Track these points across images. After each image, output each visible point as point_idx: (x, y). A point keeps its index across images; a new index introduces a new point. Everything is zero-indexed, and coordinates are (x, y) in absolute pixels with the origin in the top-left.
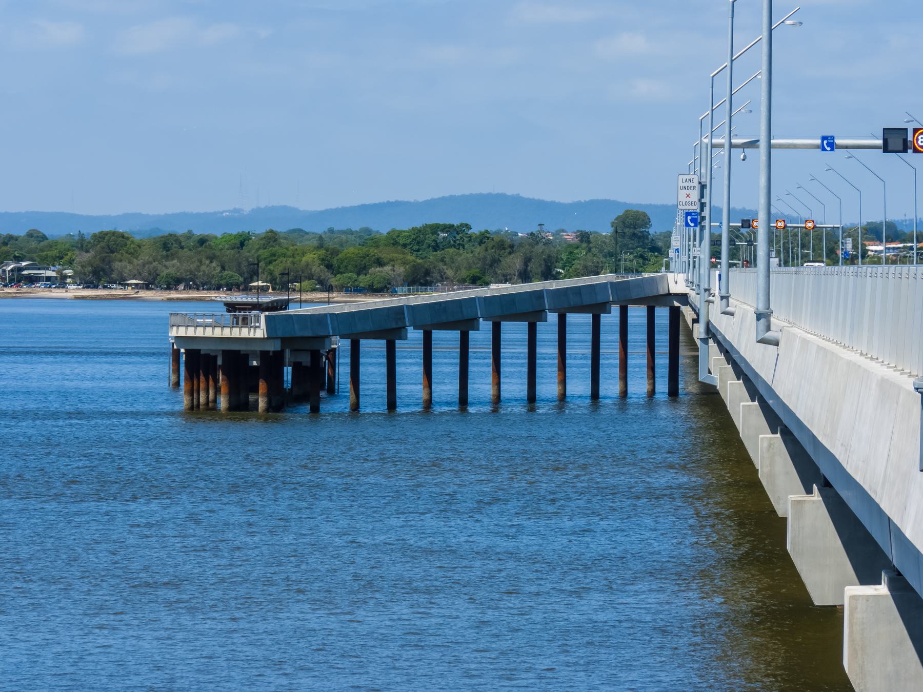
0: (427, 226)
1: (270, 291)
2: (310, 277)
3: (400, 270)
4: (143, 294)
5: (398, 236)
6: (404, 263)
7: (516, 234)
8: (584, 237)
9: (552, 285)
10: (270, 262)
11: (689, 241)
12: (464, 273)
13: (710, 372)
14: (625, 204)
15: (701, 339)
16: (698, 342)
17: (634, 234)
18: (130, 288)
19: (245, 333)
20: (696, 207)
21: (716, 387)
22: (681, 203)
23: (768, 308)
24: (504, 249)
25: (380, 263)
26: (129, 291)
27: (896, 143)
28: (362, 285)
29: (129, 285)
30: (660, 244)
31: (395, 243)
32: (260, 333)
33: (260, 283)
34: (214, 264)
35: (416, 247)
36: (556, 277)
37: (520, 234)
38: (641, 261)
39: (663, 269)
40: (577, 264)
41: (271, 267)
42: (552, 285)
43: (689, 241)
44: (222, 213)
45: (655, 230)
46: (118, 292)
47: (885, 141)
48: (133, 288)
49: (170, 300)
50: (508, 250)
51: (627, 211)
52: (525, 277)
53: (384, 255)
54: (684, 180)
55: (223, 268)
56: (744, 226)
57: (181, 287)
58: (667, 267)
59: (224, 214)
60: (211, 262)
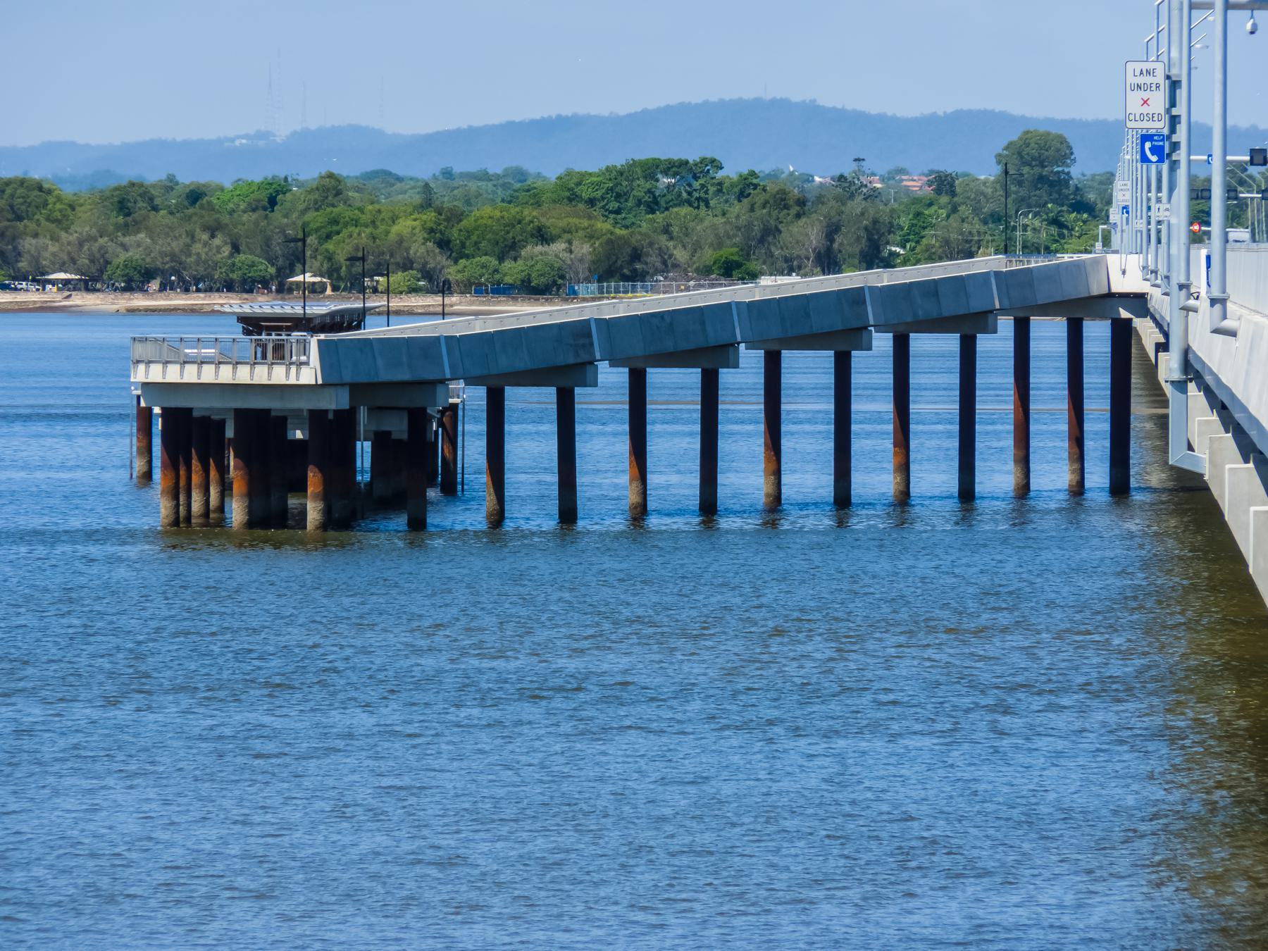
0: (634, 164)
1: (329, 291)
2: (406, 265)
3: (584, 249)
4: (80, 300)
7: (809, 178)
8: (944, 184)
9: (882, 278)
10: (329, 237)
11: (1149, 191)
12: (708, 255)
13: (1190, 448)
14: (1023, 119)
15: (1172, 382)
16: (1168, 389)
19: (279, 375)
20: (1160, 124)
21: (1202, 475)
22: (1132, 117)
24: (787, 207)
25: (543, 236)
27: (1257, 159)
29: (53, 283)
31: (573, 198)
33: (309, 278)
34: (217, 241)
35: (614, 205)
36: (888, 263)
37: (817, 179)
39: (1099, 245)
40: (931, 238)
41: (330, 246)
42: (882, 278)
43: (1149, 191)
44: (233, 140)
45: (1080, 170)
50: (793, 211)
51: (1027, 132)
52: (828, 262)
53: (554, 219)
54: (1138, 73)
55: (236, 249)
56: (1255, 162)
59: (237, 143)
60: (213, 236)
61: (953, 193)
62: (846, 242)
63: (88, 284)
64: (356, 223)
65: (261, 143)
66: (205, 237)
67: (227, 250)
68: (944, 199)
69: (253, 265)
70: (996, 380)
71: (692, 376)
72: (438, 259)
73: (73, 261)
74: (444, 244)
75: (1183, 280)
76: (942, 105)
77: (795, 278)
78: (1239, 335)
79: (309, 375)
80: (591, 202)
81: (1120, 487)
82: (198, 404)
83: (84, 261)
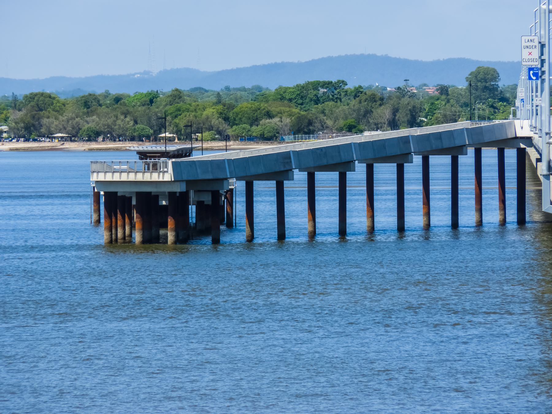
0: (309, 83)
1: (176, 140)
2: (210, 129)
3: (287, 121)
4: (68, 145)
5: (285, 92)
6: (290, 115)
7: (385, 89)
8: (444, 90)
9: (417, 131)
10: (176, 117)
12: (341, 123)
14: (478, 62)
15: (543, 175)
16: (541, 178)
18: (57, 141)
19: (155, 177)
24: (375, 101)
25: (269, 115)
26: (56, 143)
28: (254, 134)
29: (55, 138)
31: (282, 98)
32: (168, 177)
33: (168, 135)
34: (128, 119)
36: (420, 125)
37: (388, 89)
38: (492, 110)
39: (511, 116)
40: (438, 114)
41: (177, 120)
42: (417, 131)
43: (532, 92)
44: (134, 75)
45: (503, 83)
46: (46, 144)
48: (59, 141)
49: (91, 150)
50: (378, 103)
51: (479, 68)
52: (394, 125)
55: (136, 122)
57: (100, 139)
58: (515, 114)
59: (136, 76)
60: (126, 117)
62: (402, 116)
63: (71, 138)
67: (132, 123)
69: (143, 129)
72: (224, 126)
73: (65, 128)
74: (226, 119)
75: (547, 131)
77: (379, 132)
79: (168, 177)
80: (290, 100)
81: (521, 221)
82: (121, 191)
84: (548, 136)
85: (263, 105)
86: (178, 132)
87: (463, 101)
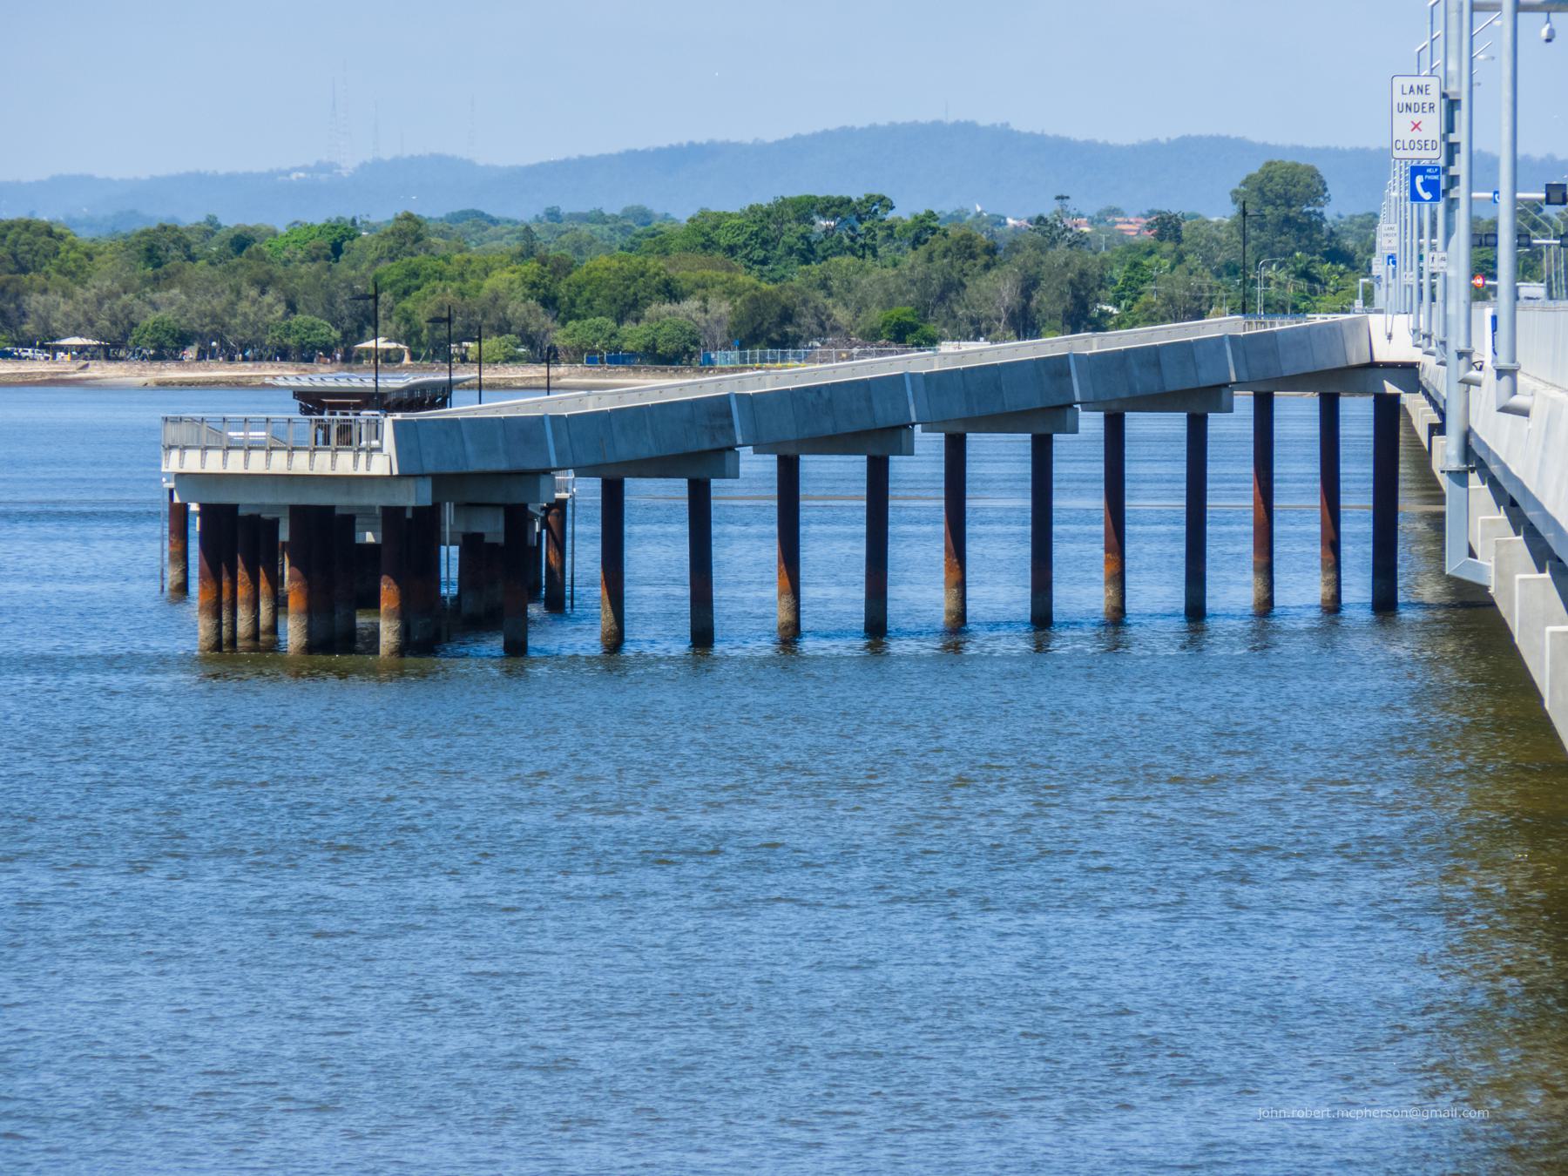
1: (407, 361)
2: (503, 328)
3: (722, 308)
4: (99, 370)
7: (1000, 221)
8: (1167, 227)
9: (1090, 344)
11: (1421, 236)
12: (876, 316)
13: (1472, 554)
14: (1265, 147)
16: (1444, 482)
17: (1288, 220)
19: (345, 464)
21: (1486, 588)
23: (1514, 361)
24: (973, 256)
25: (671, 292)
28: (628, 346)
29: (66, 349)
30: (1350, 243)
31: (709, 245)
33: (382, 344)
34: (268, 299)
35: (759, 254)
36: (1098, 325)
37: (1010, 221)
38: (1303, 284)
39: (1359, 303)
40: (1151, 295)
41: (408, 304)
42: (1090, 344)
43: (1421, 236)
44: (288, 173)
45: (1336, 210)
47: (1548, 195)
50: (981, 261)
52: (1024, 324)
53: (685, 271)
55: (292, 307)
56: (1552, 200)
58: (1368, 299)
59: (294, 176)
60: (263, 292)
61: (1179, 239)
62: (1046, 300)
63: (110, 351)
64: (440, 276)
65: (323, 177)
66: (254, 293)
67: (280, 310)
68: (1168, 246)
69: (313, 328)
70: (1231, 470)
71: (856, 465)
72: (542, 321)
73: (91, 323)
74: (549, 302)
75: (1462, 347)
76: (1167, 130)
78: (1532, 414)
79: (382, 464)
80: (731, 250)
81: (1385, 603)
83: (103, 323)
84: (1464, 360)
85: (654, 263)
86: (411, 337)
87: (1221, 257)
